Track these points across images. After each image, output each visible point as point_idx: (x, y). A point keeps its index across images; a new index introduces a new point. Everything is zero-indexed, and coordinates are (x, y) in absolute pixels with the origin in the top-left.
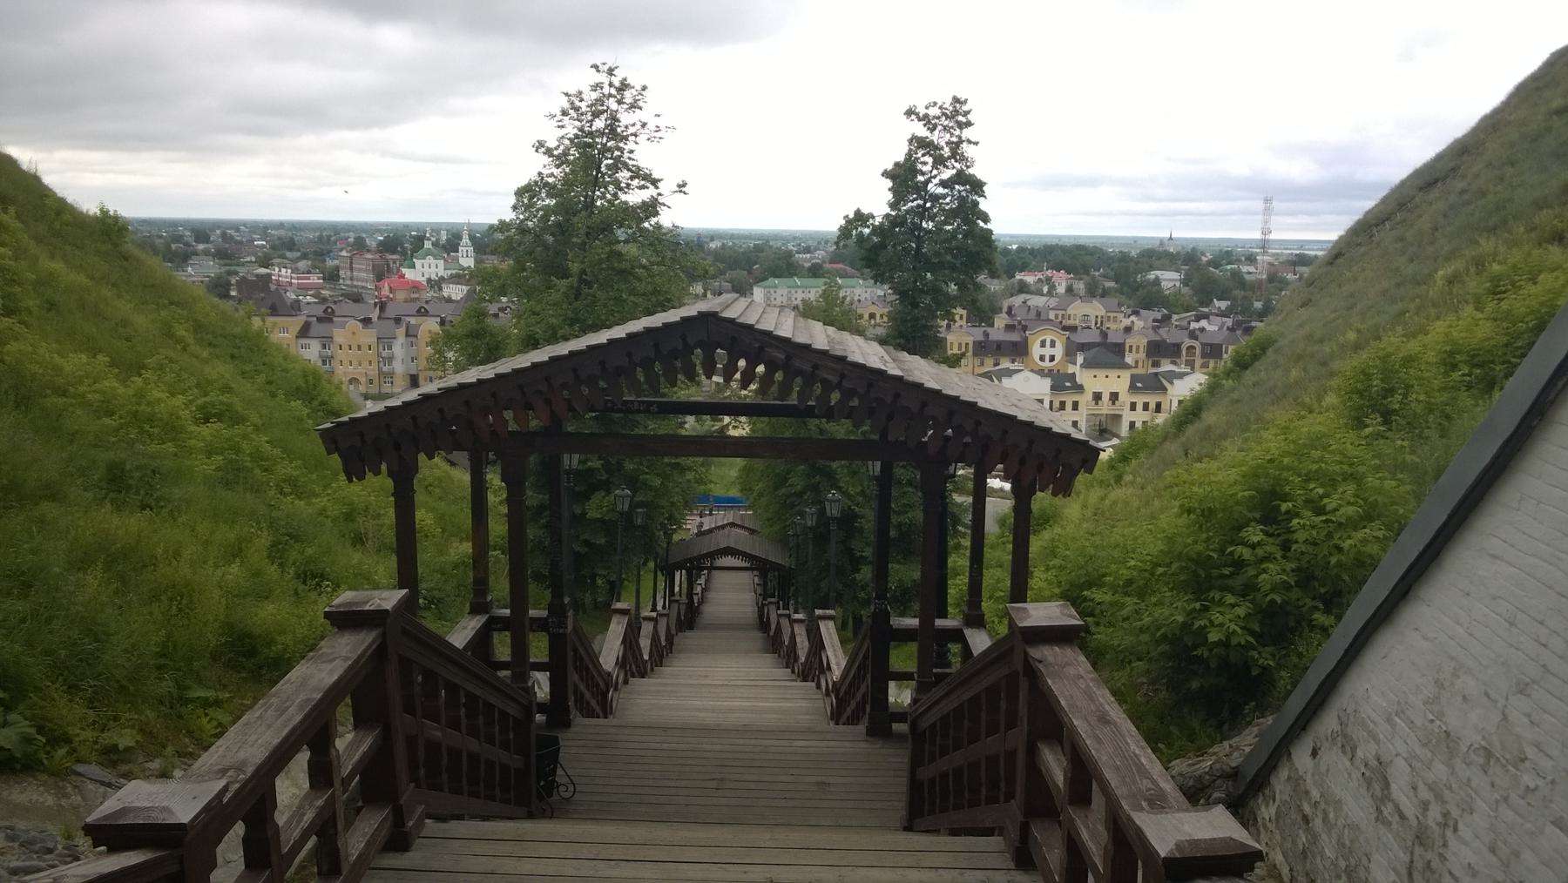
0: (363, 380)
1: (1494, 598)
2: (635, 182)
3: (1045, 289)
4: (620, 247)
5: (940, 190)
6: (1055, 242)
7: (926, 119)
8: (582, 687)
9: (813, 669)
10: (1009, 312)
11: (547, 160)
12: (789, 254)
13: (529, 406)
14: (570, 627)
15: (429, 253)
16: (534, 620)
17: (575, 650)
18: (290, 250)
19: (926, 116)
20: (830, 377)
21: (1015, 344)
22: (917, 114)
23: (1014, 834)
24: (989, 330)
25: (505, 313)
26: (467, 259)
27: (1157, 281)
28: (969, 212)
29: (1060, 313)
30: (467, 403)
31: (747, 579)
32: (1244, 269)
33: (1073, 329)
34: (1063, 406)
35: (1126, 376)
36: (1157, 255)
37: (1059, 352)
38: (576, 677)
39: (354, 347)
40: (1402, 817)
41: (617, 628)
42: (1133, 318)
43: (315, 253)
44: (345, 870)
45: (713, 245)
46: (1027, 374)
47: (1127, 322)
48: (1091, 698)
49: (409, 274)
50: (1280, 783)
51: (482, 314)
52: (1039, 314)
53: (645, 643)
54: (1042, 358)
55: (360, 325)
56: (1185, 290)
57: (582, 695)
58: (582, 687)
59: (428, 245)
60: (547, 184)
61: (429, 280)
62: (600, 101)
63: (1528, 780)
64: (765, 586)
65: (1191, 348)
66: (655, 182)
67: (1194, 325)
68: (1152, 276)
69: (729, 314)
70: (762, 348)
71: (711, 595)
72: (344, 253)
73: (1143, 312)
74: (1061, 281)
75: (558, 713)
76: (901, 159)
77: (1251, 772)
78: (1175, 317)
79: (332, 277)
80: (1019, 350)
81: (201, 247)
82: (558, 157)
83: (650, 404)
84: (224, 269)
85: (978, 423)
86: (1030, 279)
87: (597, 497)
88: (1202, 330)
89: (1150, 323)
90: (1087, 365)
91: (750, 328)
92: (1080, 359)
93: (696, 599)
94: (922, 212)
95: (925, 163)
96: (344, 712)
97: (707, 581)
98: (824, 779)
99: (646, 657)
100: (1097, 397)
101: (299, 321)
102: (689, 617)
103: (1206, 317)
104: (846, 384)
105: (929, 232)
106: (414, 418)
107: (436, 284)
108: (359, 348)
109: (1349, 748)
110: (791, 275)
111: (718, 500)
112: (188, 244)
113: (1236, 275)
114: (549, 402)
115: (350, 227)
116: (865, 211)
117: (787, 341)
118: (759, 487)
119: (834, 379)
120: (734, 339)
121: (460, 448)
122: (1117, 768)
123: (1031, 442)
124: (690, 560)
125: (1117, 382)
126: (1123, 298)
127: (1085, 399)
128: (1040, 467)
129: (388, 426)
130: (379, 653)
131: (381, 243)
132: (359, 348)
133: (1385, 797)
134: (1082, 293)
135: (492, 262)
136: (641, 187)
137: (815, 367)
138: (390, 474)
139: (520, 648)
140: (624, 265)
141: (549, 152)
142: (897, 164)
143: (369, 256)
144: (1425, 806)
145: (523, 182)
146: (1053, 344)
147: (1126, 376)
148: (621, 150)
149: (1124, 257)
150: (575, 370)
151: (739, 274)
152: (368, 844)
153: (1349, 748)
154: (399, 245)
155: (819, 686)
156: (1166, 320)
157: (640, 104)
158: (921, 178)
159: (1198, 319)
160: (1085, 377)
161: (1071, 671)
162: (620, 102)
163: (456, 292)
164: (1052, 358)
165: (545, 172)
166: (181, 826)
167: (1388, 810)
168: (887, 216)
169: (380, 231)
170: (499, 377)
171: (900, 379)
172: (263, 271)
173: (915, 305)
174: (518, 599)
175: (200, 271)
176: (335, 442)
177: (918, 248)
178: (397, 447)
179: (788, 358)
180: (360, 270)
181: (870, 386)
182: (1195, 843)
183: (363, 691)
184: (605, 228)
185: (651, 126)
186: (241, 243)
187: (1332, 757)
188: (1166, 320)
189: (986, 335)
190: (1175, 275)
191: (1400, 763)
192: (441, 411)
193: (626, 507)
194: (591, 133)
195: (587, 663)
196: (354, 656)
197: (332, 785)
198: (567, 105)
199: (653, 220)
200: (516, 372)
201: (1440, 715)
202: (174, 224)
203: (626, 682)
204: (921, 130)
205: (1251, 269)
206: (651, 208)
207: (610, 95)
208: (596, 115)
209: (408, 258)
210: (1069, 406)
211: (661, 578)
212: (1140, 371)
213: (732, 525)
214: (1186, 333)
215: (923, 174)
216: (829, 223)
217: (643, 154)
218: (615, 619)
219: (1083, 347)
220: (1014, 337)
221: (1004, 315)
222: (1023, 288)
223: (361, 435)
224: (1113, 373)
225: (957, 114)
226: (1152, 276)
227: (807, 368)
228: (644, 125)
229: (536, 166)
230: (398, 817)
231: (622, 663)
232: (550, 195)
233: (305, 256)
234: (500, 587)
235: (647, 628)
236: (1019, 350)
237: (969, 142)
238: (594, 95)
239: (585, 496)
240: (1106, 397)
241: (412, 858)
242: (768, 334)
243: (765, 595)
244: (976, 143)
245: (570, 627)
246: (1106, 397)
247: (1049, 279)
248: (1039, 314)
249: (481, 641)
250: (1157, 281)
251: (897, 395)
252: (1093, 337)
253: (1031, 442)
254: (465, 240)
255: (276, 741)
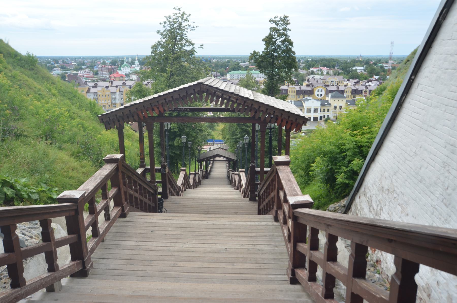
0: (107, 105)
1: (392, 152)
2: (187, 44)
3: (320, 73)
4: (182, 63)
5: (280, 44)
6: (323, 58)
7: (275, 22)
8: (171, 189)
9: (238, 187)
10: (308, 81)
11: (160, 36)
12: (239, 63)
13: (153, 110)
14: (167, 171)
15: (125, 65)
16: (157, 169)
17: (169, 178)
18: (83, 65)
19: (275, 21)
20: (234, 100)
21: (310, 91)
22: (273, 21)
23: (274, 213)
24: (301, 86)
25: (148, 84)
26: (137, 67)
27: (356, 70)
28: (288, 51)
29: (324, 81)
30: (137, 109)
31: (225, 165)
32: (385, 65)
33: (328, 86)
34: (324, 110)
35: (344, 100)
36: (356, 62)
37: (323, 93)
38: (169, 186)
39: (104, 95)
40: (374, 209)
41: (182, 175)
42: (348, 82)
43: (91, 66)
44: (111, 219)
45: (214, 61)
46: (313, 100)
47: (345, 83)
48: (288, 176)
49: (120, 72)
50: (353, 207)
51: (141, 86)
52: (317, 81)
53: (191, 181)
54: (318, 95)
55: (105, 88)
56: (365, 73)
57: (171, 191)
58: (171, 189)
59: (125, 63)
60: (161, 44)
61: (126, 74)
62: (176, 19)
63: (395, 195)
64: (229, 166)
65: (365, 91)
66: (193, 44)
67: (367, 84)
68: (354, 68)
69: (206, 83)
70: (215, 92)
71: (213, 170)
72: (100, 66)
73: (351, 80)
74: (325, 70)
75: (165, 195)
76: (268, 35)
77: (346, 205)
78: (361, 81)
79: (96, 73)
80: (311, 93)
81: (56, 65)
82: (164, 35)
83: (188, 109)
84: (64, 72)
85: (274, 112)
86: (315, 70)
87: (177, 139)
88: (370, 85)
89: (353, 83)
90: (332, 97)
91: (212, 87)
92: (330, 95)
93: (208, 170)
94: (274, 50)
95: (275, 35)
96: (109, 183)
97: (212, 165)
98: (237, 211)
99: (191, 184)
100: (335, 107)
101: (87, 88)
102: (206, 175)
103: (371, 81)
104: (238, 102)
105: (276, 56)
106: (123, 113)
107: (128, 75)
108: (105, 96)
109: (365, 195)
110: (239, 70)
111: (216, 141)
112: (52, 64)
113: (382, 67)
114: (158, 108)
115: (101, 58)
116: (257, 51)
117: (222, 90)
118: (227, 137)
119: (235, 100)
120: (208, 90)
121: (135, 121)
122: (289, 190)
123: (289, 117)
124: (207, 158)
125: (342, 103)
126: (345, 76)
127: (332, 108)
128: (292, 124)
129: (116, 115)
130: (117, 169)
131: (111, 63)
132: (105, 96)
133: (371, 206)
134: (332, 74)
135: (144, 68)
136: (188, 45)
137: (230, 97)
138: (117, 128)
139: (153, 177)
140: (184, 70)
141: (162, 34)
142: (266, 37)
143: (107, 67)
144: (378, 205)
145: (154, 44)
146: (322, 91)
147: (344, 100)
148: (182, 33)
149: (346, 62)
150: (165, 99)
151: (223, 69)
152: (116, 214)
153: (365, 195)
154: (116, 63)
155: (240, 191)
156: (358, 82)
157: (188, 19)
158: (274, 40)
159: (368, 82)
160: (331, 101)
161: (285, 171)
162: (182, 19)
163: (135, 77)
164: (321, 95)
165: (160, 40)
166: (77, 199)
167: (371, 208)
168: (263, 52)
169: (110, 59)
170: (145, 101)
171: (253, 100)
172: (75, 72)
173: (272, 79)
174: (152, 164)
175: (57, 72)
176: (102, 120)
177: (273, 62)
178: (119, 121)
179: (222, 95)
180: (105, 71)
181: (245, 102)
182: (299, 201)
183: (113, 177)
184: (178, 58)
185: (192, 26)
186: (68, 63)
187: (363, 198)
188: (358, 82)
189: (300, 88)
190: (362, 68)
191: (374, 196)
192: (130, 111)
193: (185, 141)
194: (174, 28)
195: (173, 184)
196: (111, 169)
197: (107, 199)
198: (166, 20)
199: (193, 55)
200: (149, 100)
201: (381, 183)
202: (47, 58)
203: (185, 190)
204: (274, 25)
205: (387, 65)
206: (192, 51)
207: (179, 16)
208: (175, 23)
209: (119, 67)
210: (326, 110)
211: (197, 163)
212: (349, 99)
213: (220, 148)
214: (364, 86)
215: (274, 38)
216: (247, 53)
217: (189, 35)
218: (181, 172)
219: (331, 91)
220: (309, 88)
221: (307, 82)
222: (313, 73)
223: (109, 117)
224: (340, 100)
225: (285, 20)
226: (354, 68)
227: (228, 98)
228: (189, 26)
229: (157, 38)
230: (123, 210)
231: (184, 185)
232: (162, 48)
233: (88, 67)
234: (147, 160)
235: (192, 177)
236: (311, 93)
237: (288, 29)
238: (174, 17)
239: (174, 139)
240: (338, 107)
241: (127, 219)
242: (217, 88)
243: (229, 168)
244: (290, 30)
245: (167, 171)
246: (338, 107)
247: (321, 70)
248: (317, 81)
249: (144, 173)
250: (356, 70)
251: (252, 104)
252: (334, 88)
253: (289, 117)
254: (137, 61)
255: (95, 185)
